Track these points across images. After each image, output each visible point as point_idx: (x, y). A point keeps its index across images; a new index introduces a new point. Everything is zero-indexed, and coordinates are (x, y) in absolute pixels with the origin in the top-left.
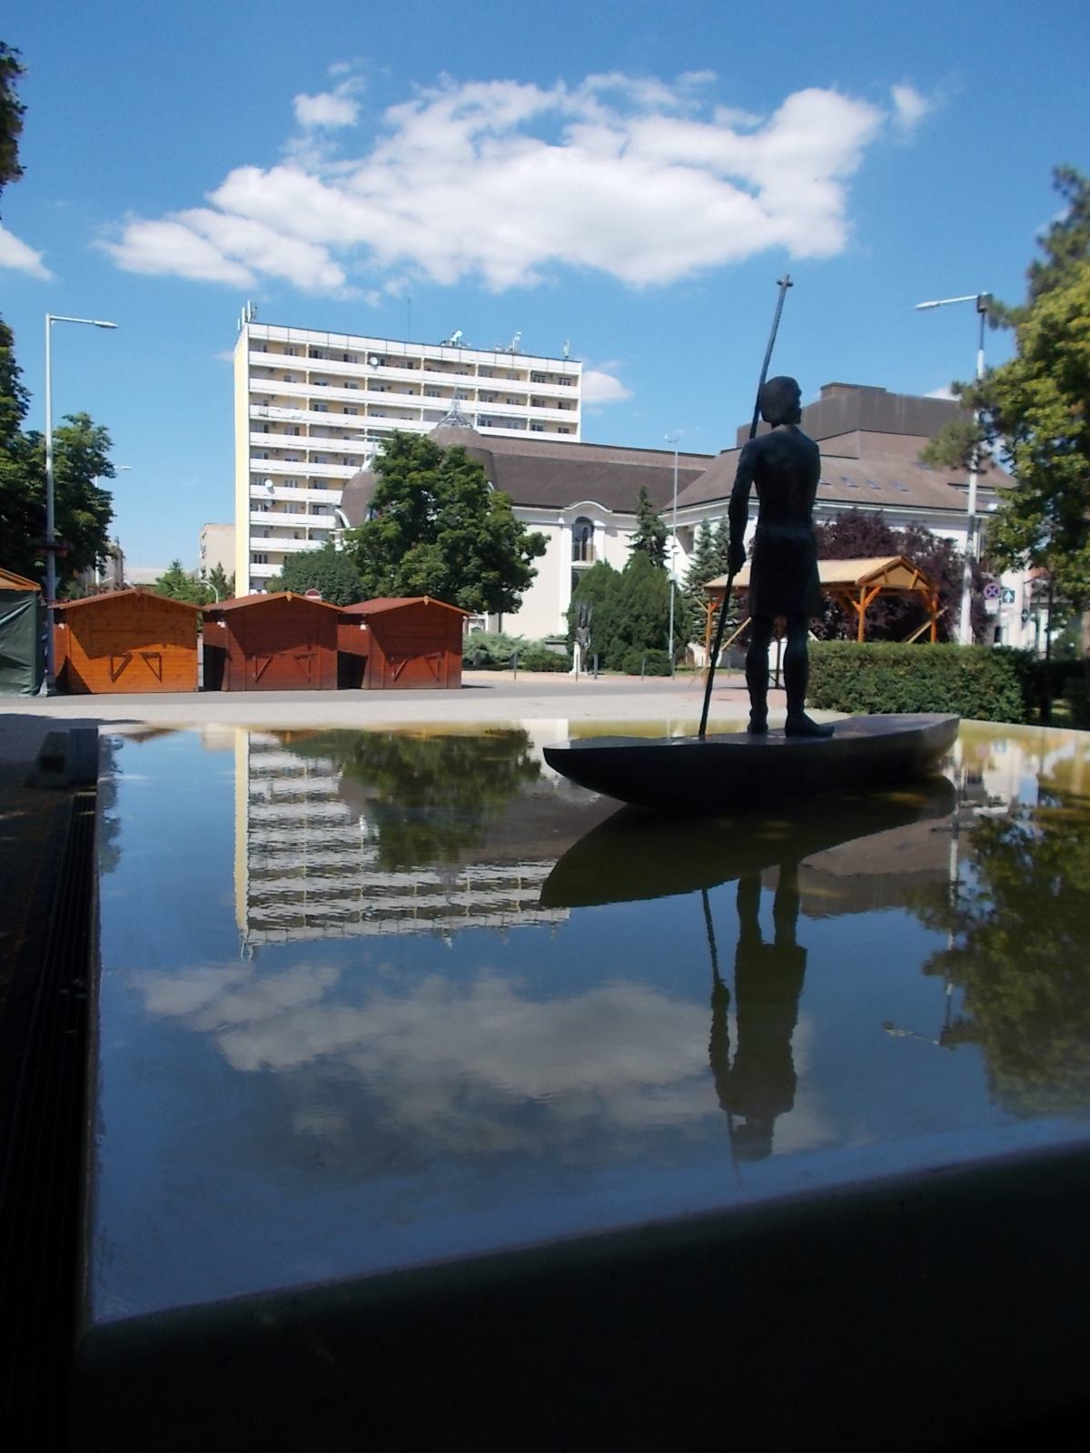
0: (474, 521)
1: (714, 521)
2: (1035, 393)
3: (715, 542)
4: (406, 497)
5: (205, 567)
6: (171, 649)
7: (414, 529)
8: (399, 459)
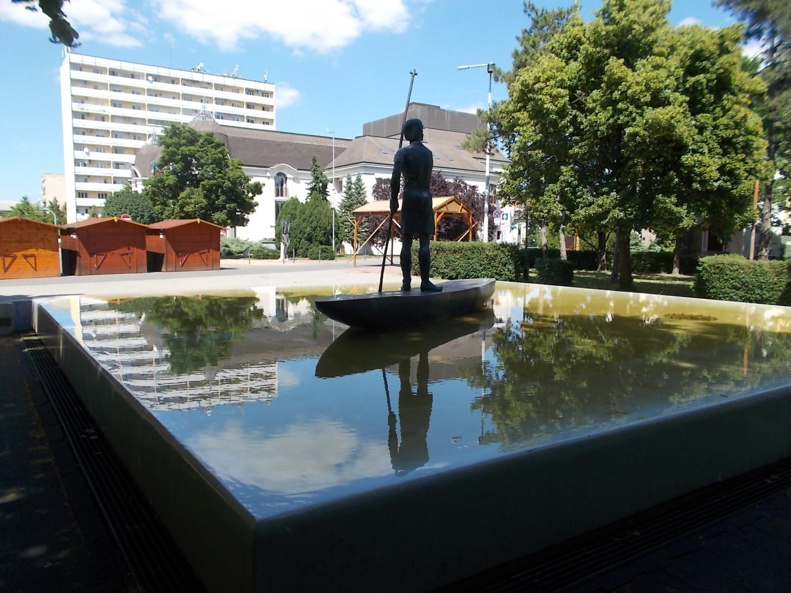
0: (221, 175)
1: (353, 175)
2: (519, 119)
3: (354, 187)
4: (179, 161)
5: (45, 200)
6: (41, 252)
7: (185, 179)
8: (174, 139)
